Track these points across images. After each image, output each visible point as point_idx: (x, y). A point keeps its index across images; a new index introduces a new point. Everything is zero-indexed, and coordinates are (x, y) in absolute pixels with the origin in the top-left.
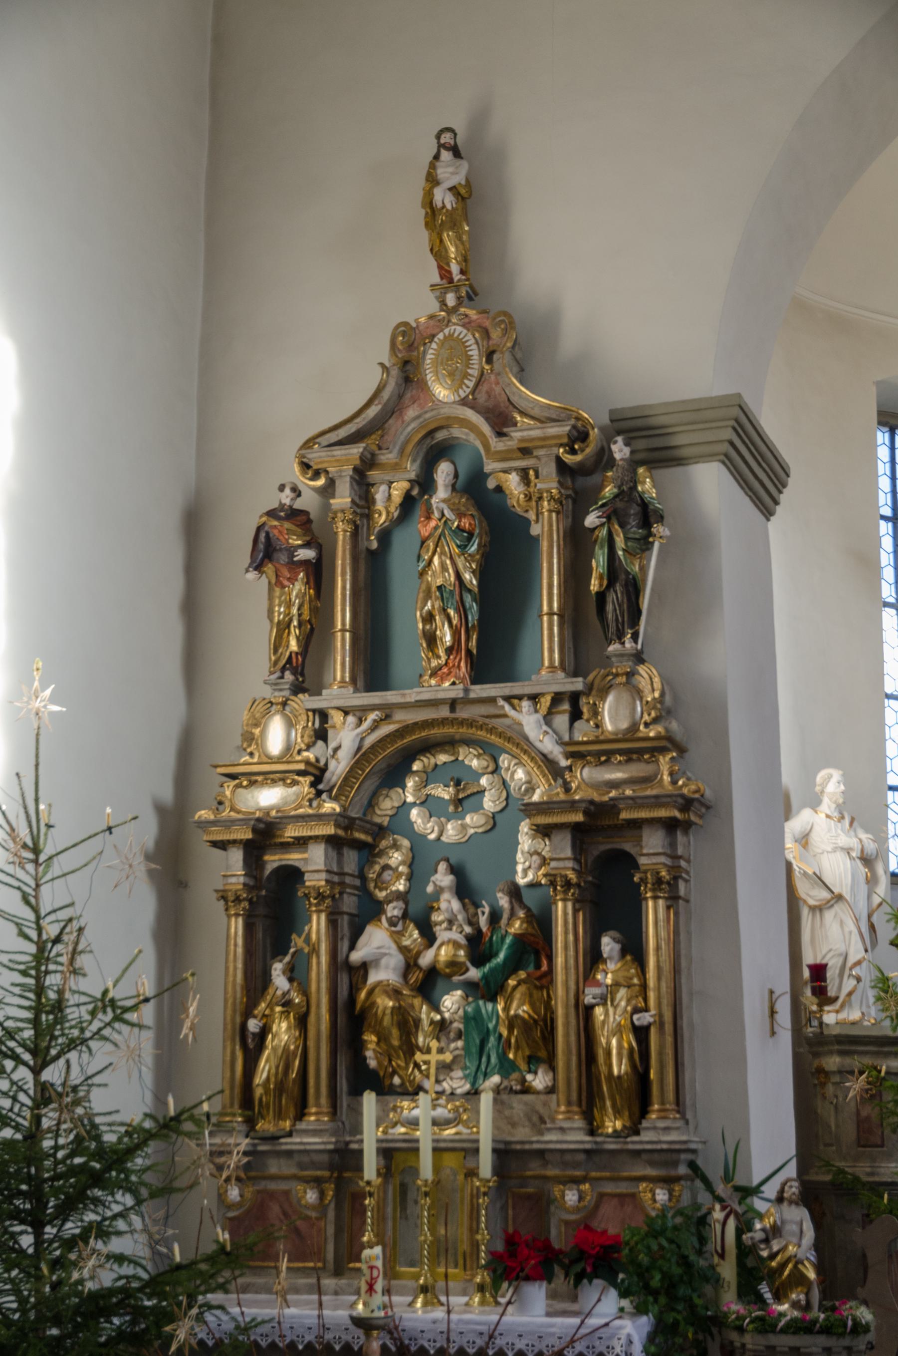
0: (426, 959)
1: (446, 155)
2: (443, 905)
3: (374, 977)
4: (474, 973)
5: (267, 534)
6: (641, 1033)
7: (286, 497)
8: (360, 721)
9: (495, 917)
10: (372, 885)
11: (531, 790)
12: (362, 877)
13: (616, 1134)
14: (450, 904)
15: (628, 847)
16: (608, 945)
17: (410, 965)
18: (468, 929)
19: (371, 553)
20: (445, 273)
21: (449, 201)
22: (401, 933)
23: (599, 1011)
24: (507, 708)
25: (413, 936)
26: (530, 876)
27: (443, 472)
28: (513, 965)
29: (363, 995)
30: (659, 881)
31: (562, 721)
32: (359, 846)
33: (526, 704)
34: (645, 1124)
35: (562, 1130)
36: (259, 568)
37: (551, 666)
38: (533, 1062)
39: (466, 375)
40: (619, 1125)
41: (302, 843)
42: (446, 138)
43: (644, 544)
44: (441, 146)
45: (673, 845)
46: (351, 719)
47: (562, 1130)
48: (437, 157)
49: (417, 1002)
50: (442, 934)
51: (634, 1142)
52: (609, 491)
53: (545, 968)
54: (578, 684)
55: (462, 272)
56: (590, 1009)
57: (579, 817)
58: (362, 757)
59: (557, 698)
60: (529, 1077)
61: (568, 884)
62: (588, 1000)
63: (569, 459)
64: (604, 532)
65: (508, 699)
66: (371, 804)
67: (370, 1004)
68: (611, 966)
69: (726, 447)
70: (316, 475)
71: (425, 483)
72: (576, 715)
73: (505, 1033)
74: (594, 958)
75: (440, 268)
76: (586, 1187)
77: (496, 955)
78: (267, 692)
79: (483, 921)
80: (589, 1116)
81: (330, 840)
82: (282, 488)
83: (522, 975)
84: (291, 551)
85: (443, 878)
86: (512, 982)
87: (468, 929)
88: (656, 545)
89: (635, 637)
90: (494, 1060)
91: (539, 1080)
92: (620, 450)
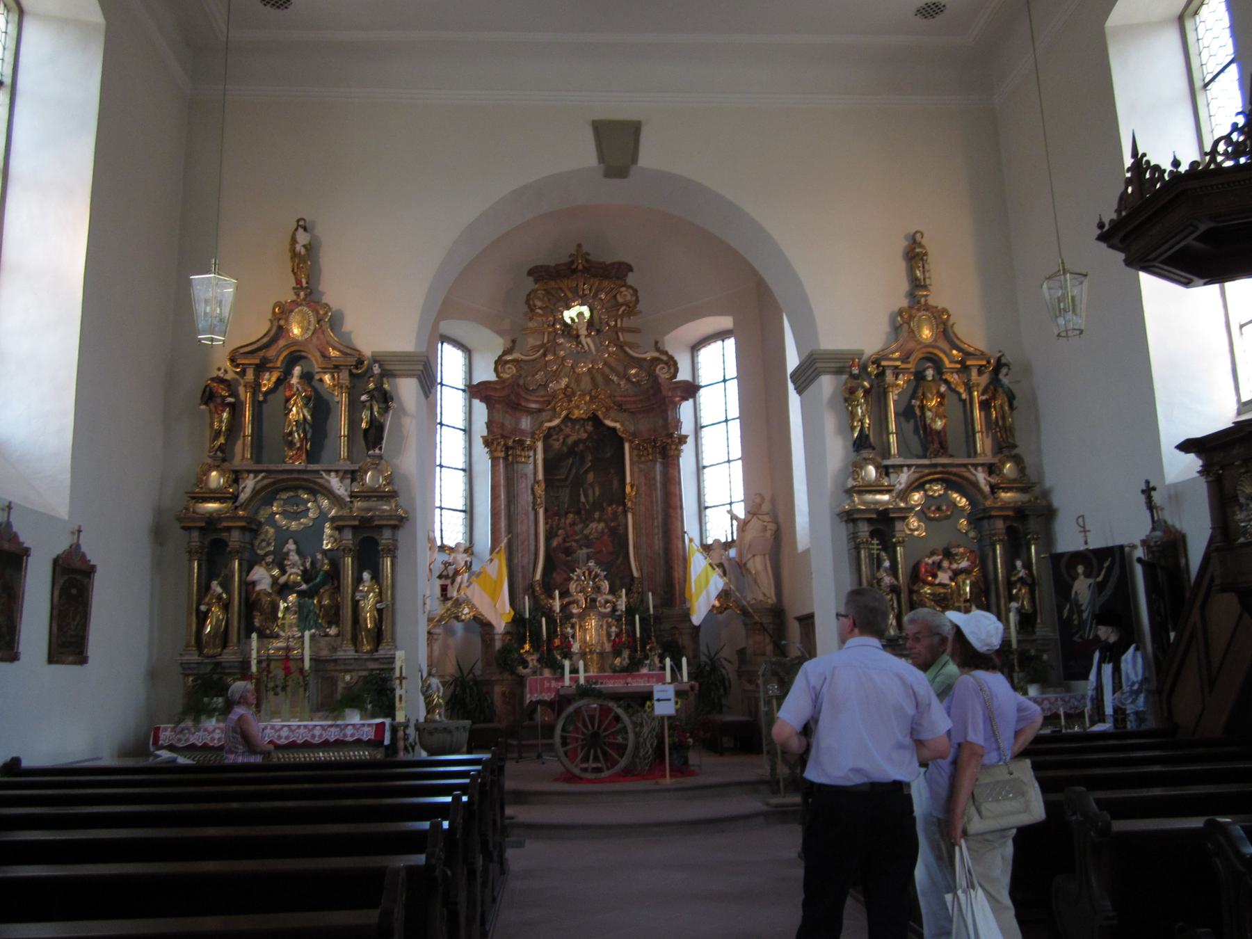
0: (283, 580)
1: (300, 230)
2: (291, 558)
3: (258, 588)
4: (304, 587)
5: (211, 389)
6: (380, 611)
7: (221, 374)
8: (255, 477)
9: (313, 564)
10: (256, 548)
11: (330, 510)
12: (252, 545)
13: (368, 652)
14: (294, 557)
15: (376, 537)
16: (366, 575)
17: (275, 580)
18: (302, 568)
19: (259, 402)
20: (298, 282)
21: (303, 251)
22: (272, 569)
23: (362, 602)
24: (324, 475)
25: (276, 572)
26: (329, 546)
27: (297, 370)
28: (323, 583)
29: (254, 596)
30: (390, 550)
31: (348, 481)
32: (252, 530)
33: (333, 474)
34: (380, 648)
35: (345, 651)
36: (206, 404)
37: (344, 458)
38: (330, 624)
39: (308, 329)
40: (368, 648)
41: (228, 529)
42: (301, 223)
43: (387, 409)
44: (298, 226)
45: (394, 535)
46: (252, 475)
47: (345, 651)
48: (296, 229)
49: (278, 598)
50: (290, 570)
51: (376, 655)
52: (371, 386)
53: (336, 582)
54: (356, 467)
55: (307, 283)
56: (358, 601)
57: (356, 523)
58: (255, 493)
59: (346, 472)
60: (328, 630)
61: (350, 550)
62: (358, 598)
63: (355, 371)
64: (368, 404)
65: (324, 471)
66: (257, 512)
67: (258, 601)
68: (366, 584)
69: (419, 373)
70: (237, 366)
71: (288, 373)
72: (353, 480)
73: (318, 612)
74: (358, 580)
75: (296, 279)
76: (353, 674)
77: (315, 579)
78: (209, 461)
79: (308, 565)
80: (355, 644)
81: (242, 528)
82: (219, 369)
83: (327, 587)
84: (224, 398)
85: (291, 546)
86: (322, 591)
87: (302, 568)
88: (391, 412)
89: (380, 449)
90: (312, 622)
91: (333, 631)
92: (376, 370)
